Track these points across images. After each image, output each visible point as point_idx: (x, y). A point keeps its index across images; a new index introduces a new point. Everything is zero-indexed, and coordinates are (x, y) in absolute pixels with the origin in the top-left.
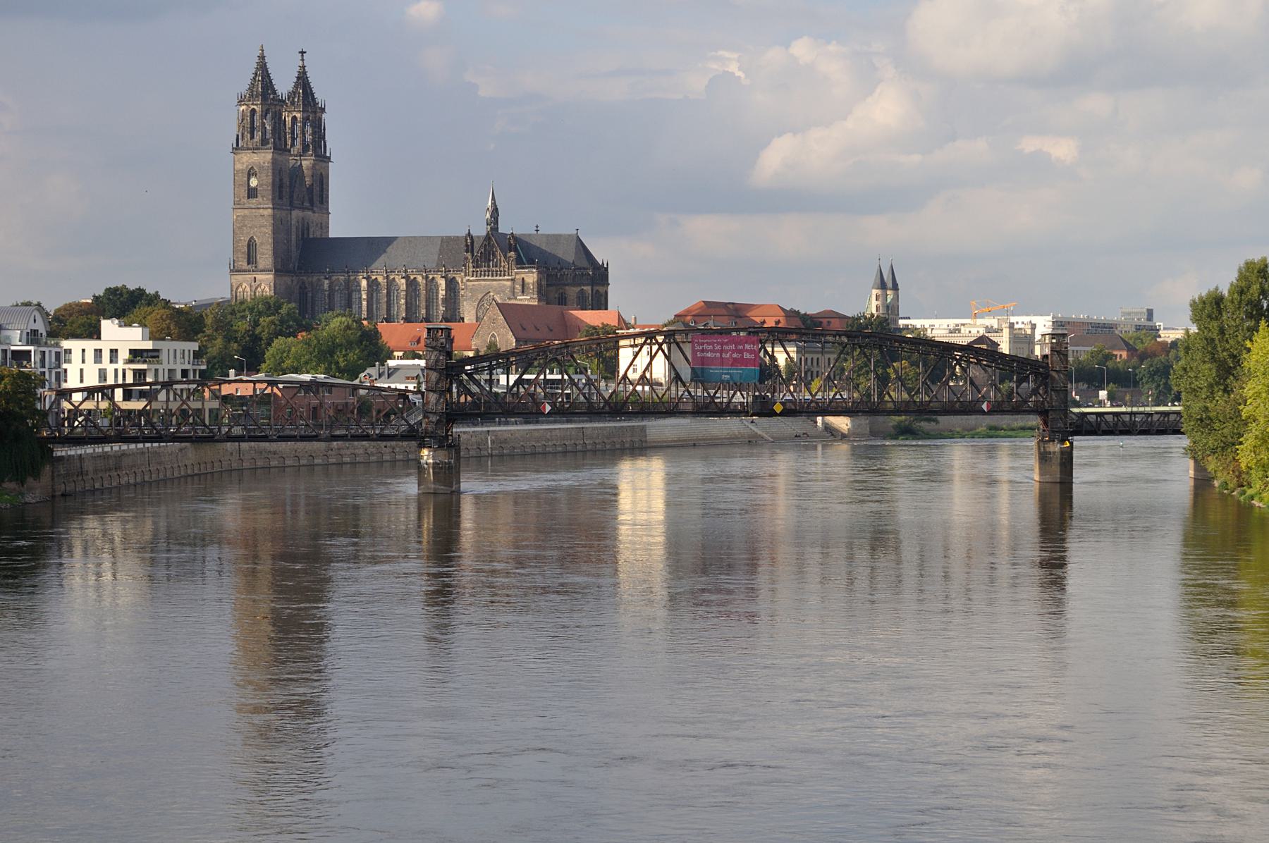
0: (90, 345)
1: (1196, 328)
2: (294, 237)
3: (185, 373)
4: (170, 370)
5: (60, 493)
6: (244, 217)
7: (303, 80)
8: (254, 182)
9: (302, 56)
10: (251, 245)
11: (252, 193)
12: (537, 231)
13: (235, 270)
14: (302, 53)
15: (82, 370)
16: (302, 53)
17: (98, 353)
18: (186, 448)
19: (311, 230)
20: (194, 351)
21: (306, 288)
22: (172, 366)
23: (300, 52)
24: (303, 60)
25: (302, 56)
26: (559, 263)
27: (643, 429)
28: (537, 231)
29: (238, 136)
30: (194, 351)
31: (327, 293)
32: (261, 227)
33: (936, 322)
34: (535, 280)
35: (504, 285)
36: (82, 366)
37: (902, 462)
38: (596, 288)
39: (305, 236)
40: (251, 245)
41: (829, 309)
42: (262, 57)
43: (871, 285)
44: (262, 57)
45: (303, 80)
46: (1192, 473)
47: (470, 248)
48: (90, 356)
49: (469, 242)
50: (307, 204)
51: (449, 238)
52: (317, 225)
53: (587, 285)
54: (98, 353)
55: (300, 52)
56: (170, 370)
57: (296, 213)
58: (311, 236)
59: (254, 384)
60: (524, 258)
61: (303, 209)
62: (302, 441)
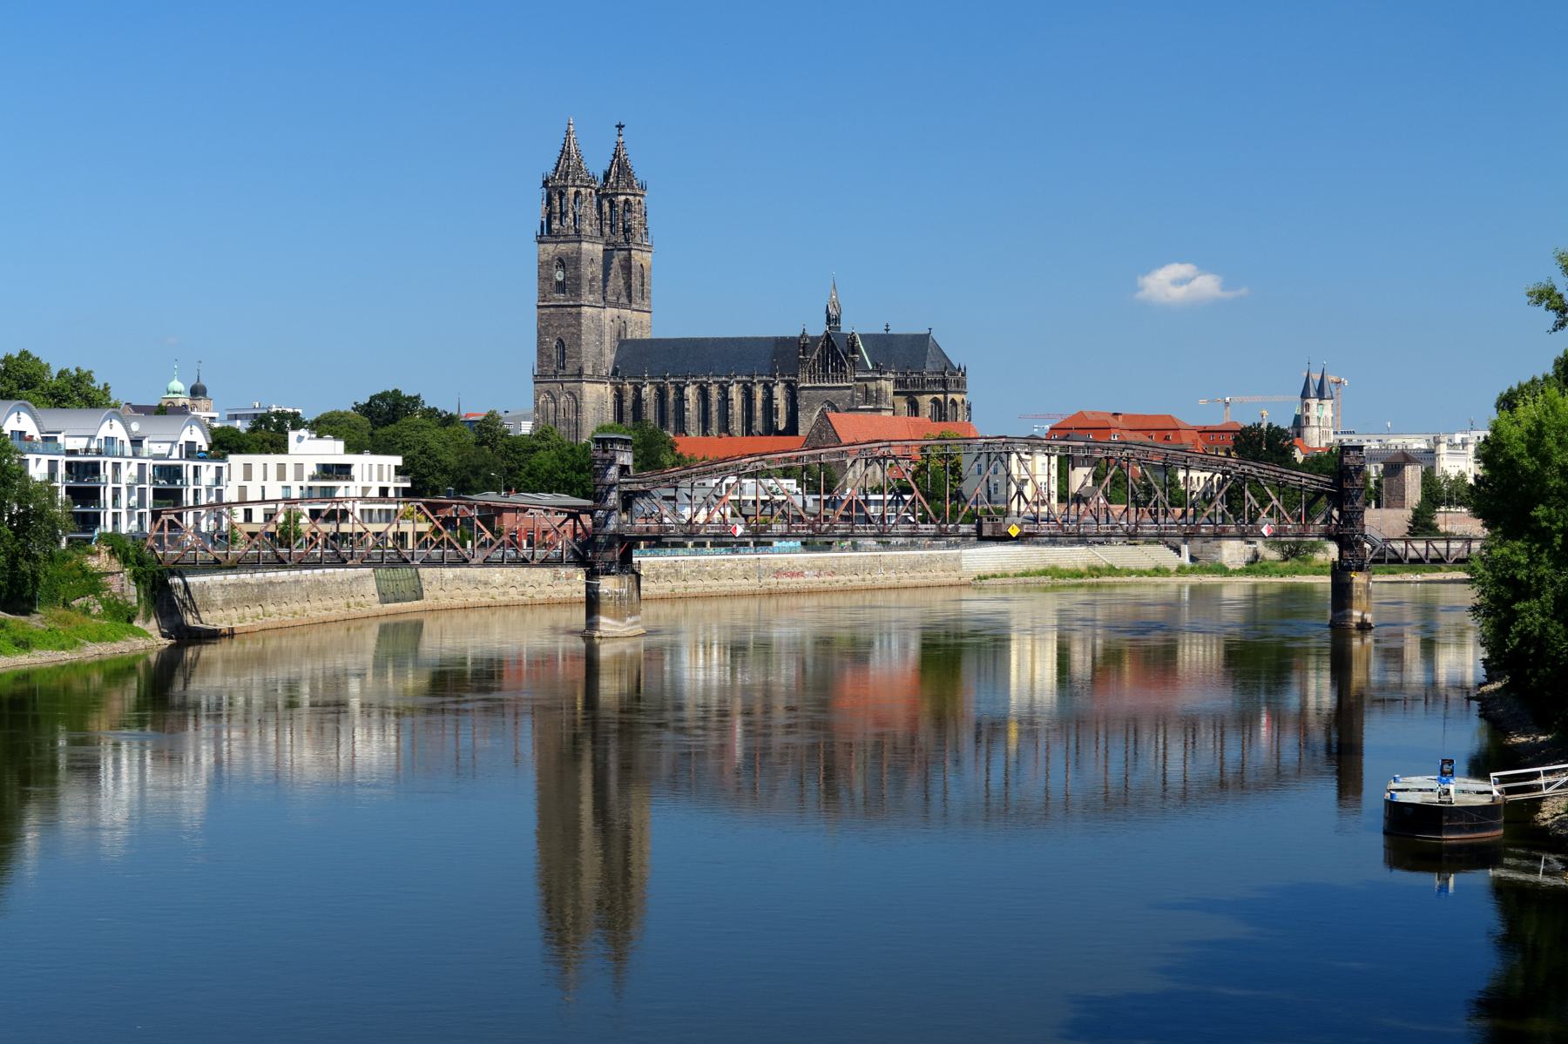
0: (273, 460)
2: (607, 338)
3: (384, 491)
4: (363, 488)
12: (887, 330)
14: (620, 127)
15: (263, 488)
16: (620, 127)
17: (281, 469)
18: (364, 576)
19: (629, 330)
20: (396, 467)
22: (367, 484)
27: (957, 559)
28: (887, 330)
29: (542, 222)
30: (396, 467)
32: (569, 326)
36: (264, 483)
37: (255, 678)
39: (623, 337)
48: (272, 472)
50: (624, 300)
51: (783, 339)
52: (636, 324)
54: (281, 469)
56: (363, 488)
57: (610, 312)
58: (629, 337)
61: (616, 305)
62: (450, 567)
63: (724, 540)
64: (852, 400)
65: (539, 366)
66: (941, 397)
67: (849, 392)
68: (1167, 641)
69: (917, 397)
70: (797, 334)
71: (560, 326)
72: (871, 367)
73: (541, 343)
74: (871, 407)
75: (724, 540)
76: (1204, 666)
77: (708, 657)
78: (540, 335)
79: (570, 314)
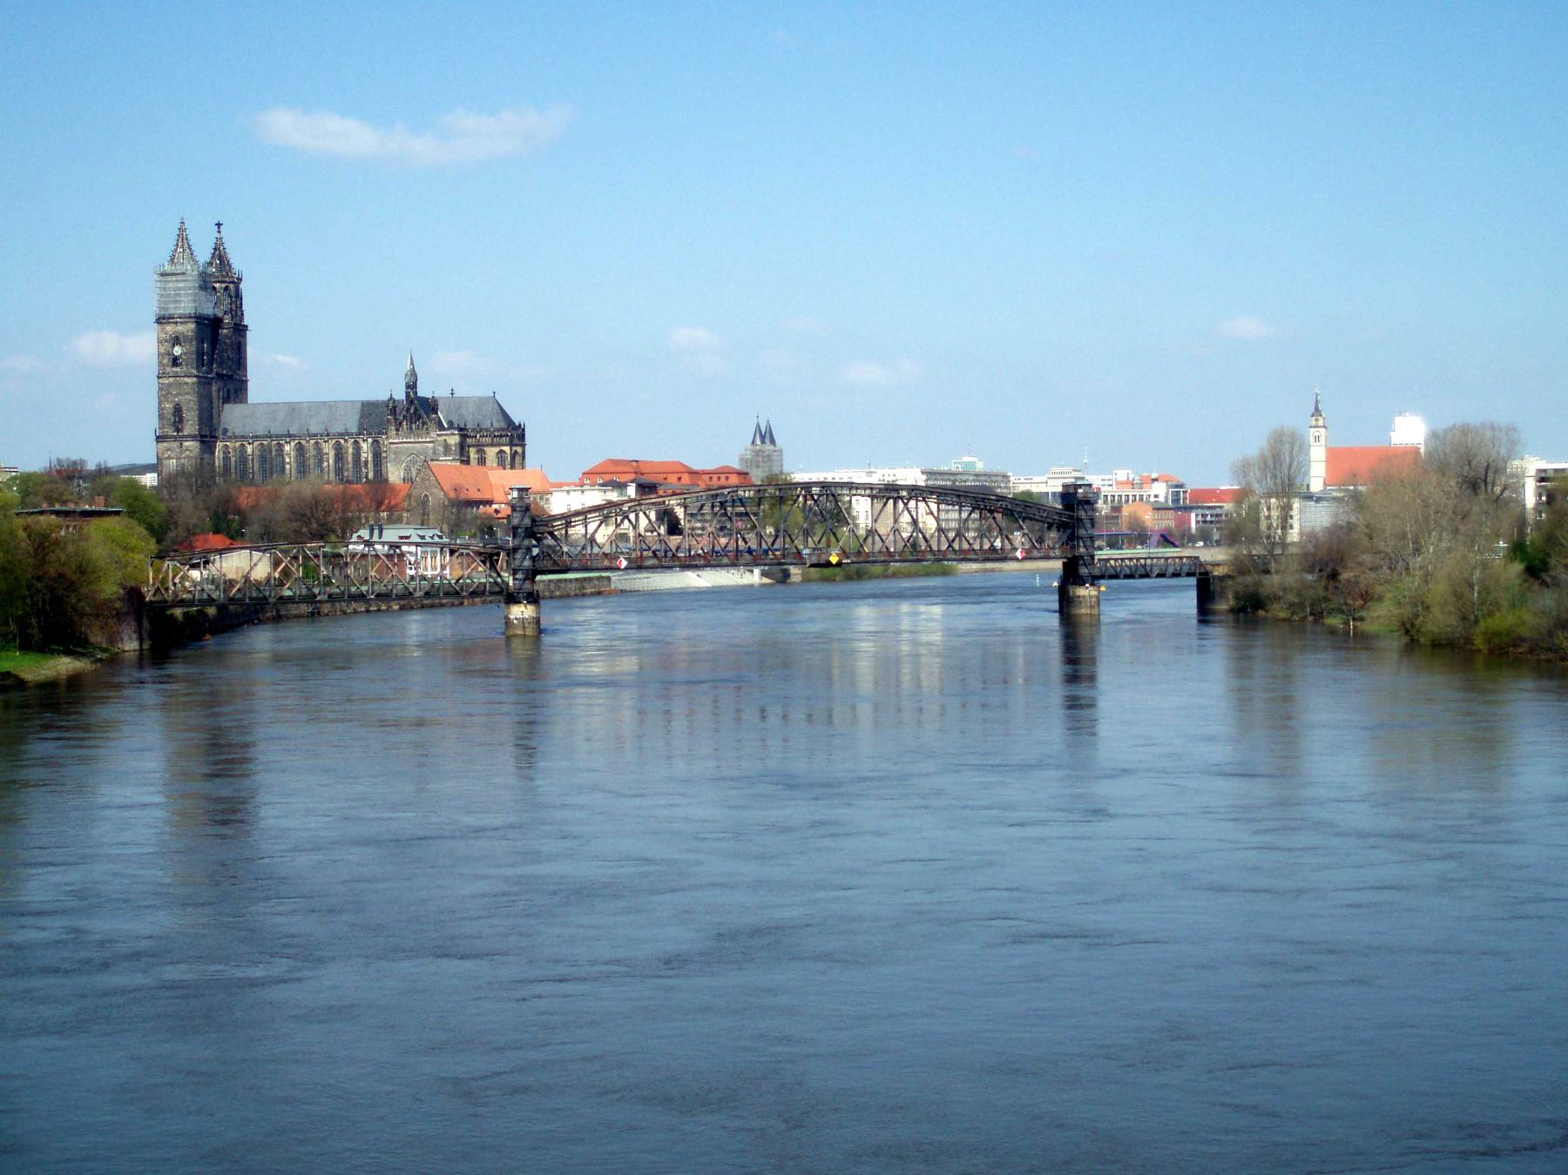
1: (491, 477)
5: (422, 593)
6: (170, 385)
7: (219, 254)
8: (177, 351)
9: (219, 227)
10: (178, 410)
11: (175, 361)
12: (452, 394)
13: (159, 439)
14: (219, 225)
16: (219, 225)
21: (229, 453)
23: (217, 224)
24: (219, 232)
25: (219, 227)
26: (478, 425)
28: (452, 394)
31: (251, 457)
33: (1096, 477)
34: (457, 441)
35: (427, 447)
38: (514, 448)
40: (178, 410)
41: (676, 459)
42: (182, 230)
43: (246, 405)
44: (182, 230)
45: (219, 254)
46: (1222, 488)
47: (393, 411)
49: (392, 407)
53: (506, 445)
55: (217, 224)
59: (872, 500)
60: (443, 420)
63: (496, 674)
64: (434, 453)
65: (160, 429)
66: (507, 449)
67: (431, 445)
68: (215, 715)
69: (489, 472)
70: (386, 397)
71: (178, 395)
72: (446, 426)
73: (161, 409)
74: (451, 458)
75: (496, 674)
76: (1501, 715)
77: (992, 591)
78: (160, 403)
79: (186, 383)
